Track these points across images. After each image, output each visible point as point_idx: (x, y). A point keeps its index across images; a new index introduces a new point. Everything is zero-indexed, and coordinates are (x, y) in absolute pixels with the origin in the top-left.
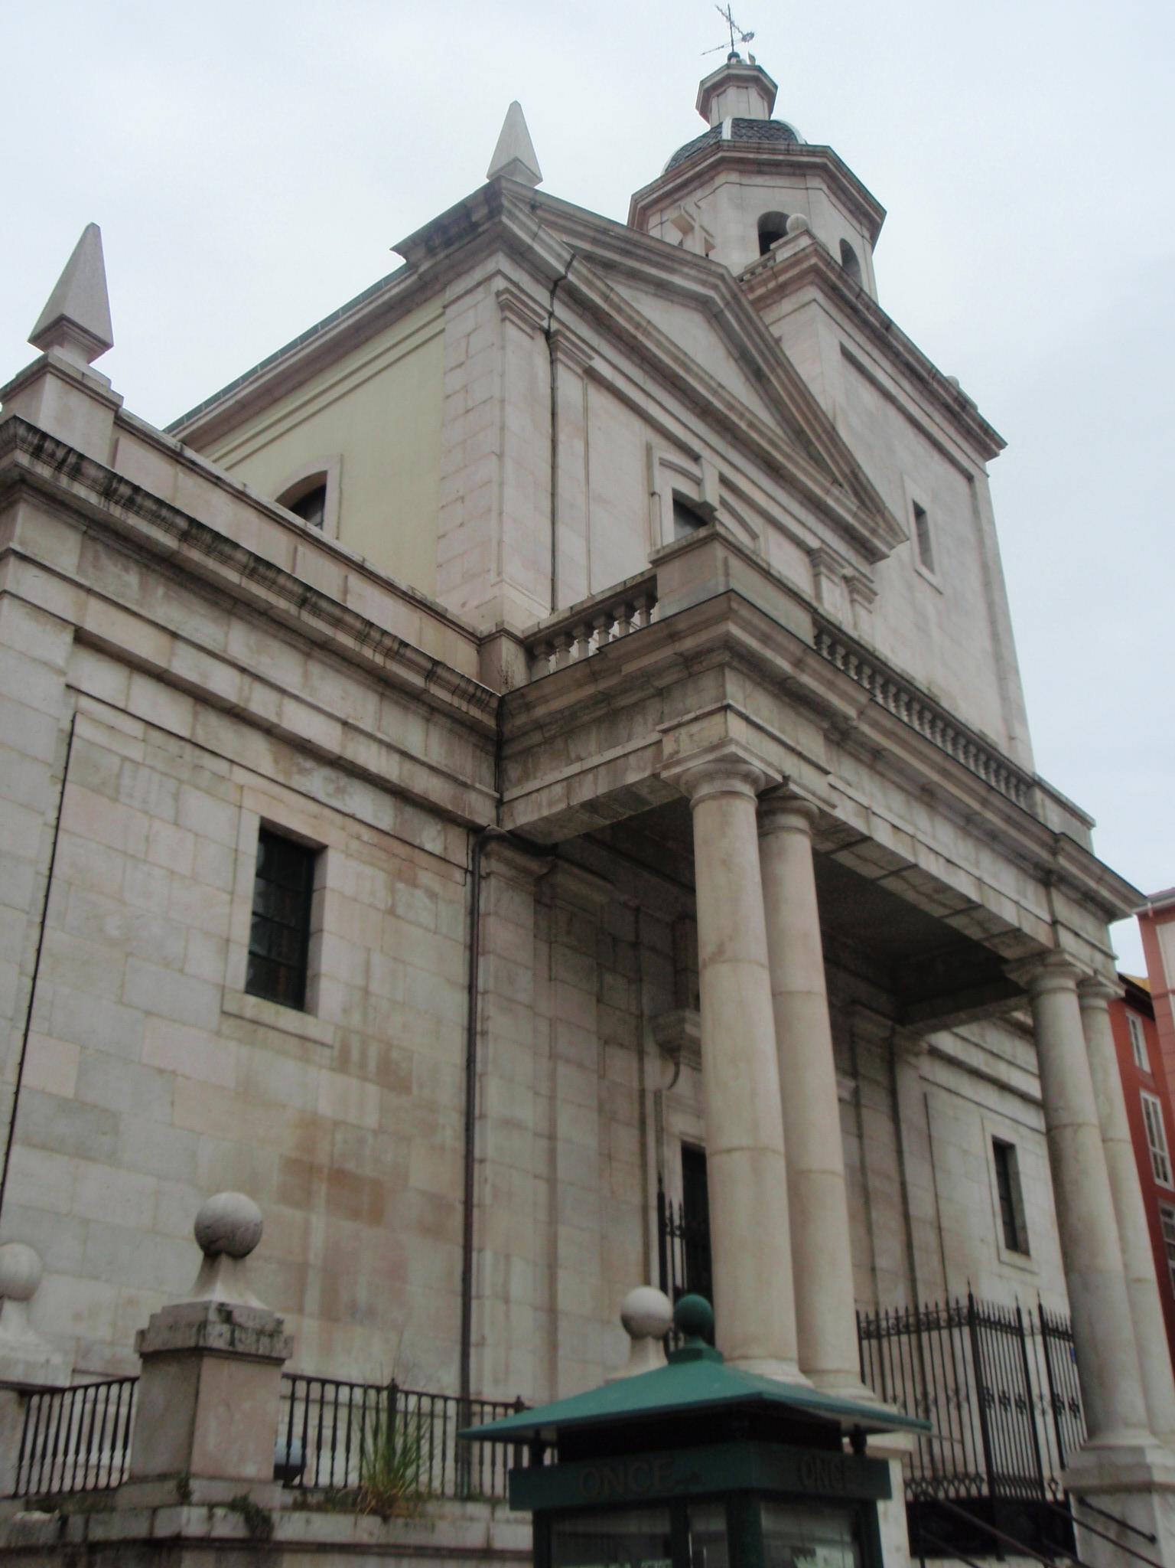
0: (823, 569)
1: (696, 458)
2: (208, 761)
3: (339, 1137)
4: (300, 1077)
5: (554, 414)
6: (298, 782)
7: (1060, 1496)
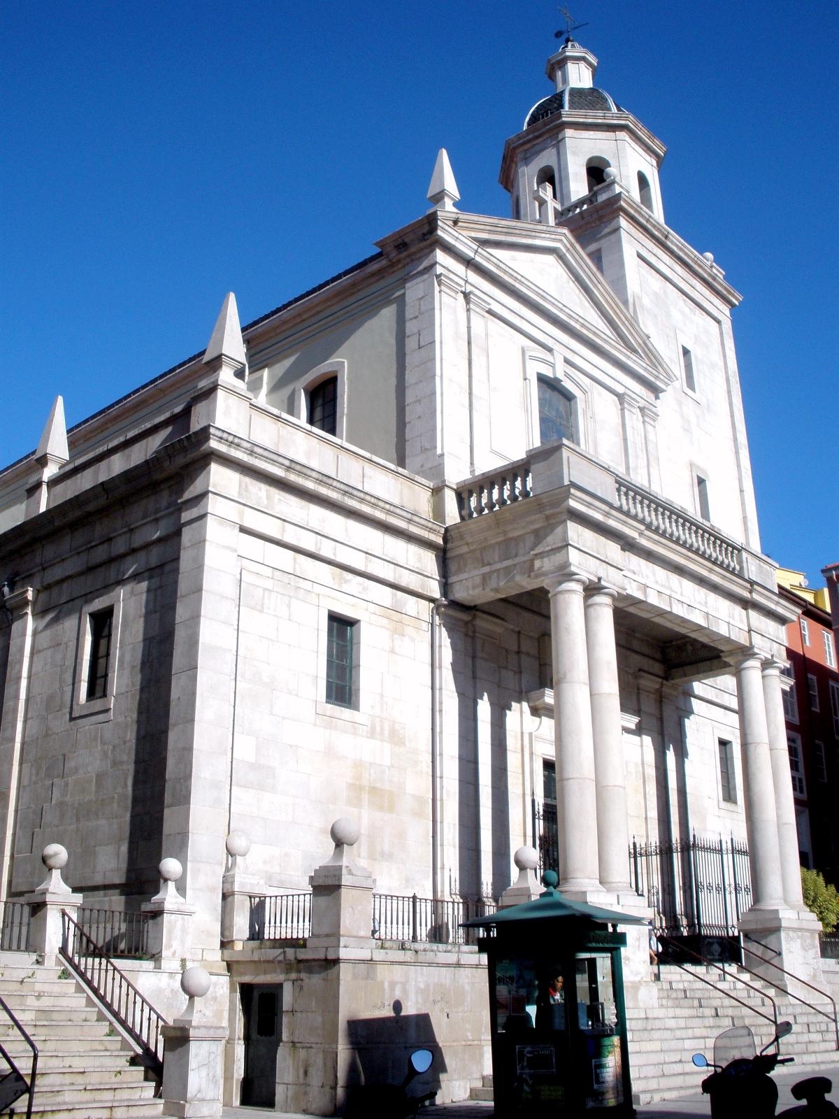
0: (626, 405)
1: (550, 350)
2: (302, 584)
3: (372, 771)
4: (348, 735)
5: (469, 343)
6: (345, 588)
7: (736, 934)
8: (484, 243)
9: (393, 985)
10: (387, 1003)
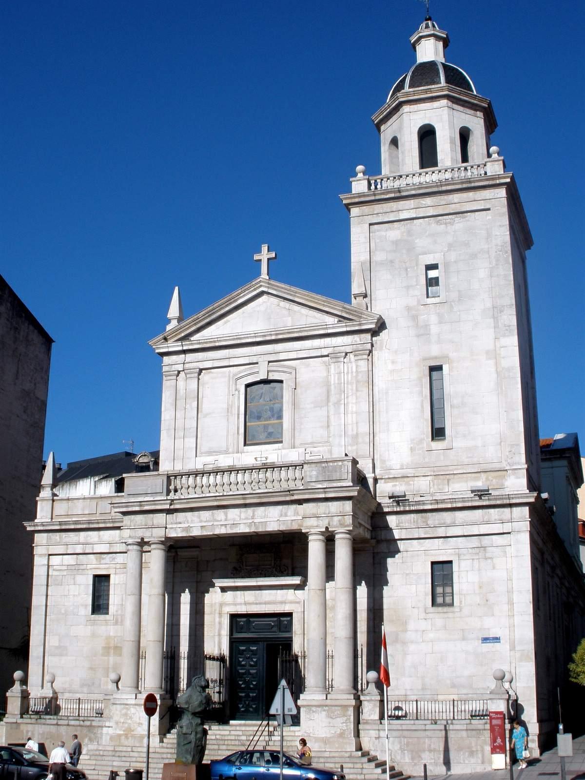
8: (186, 338)
9: (27, 732)
10: (25, 738)
